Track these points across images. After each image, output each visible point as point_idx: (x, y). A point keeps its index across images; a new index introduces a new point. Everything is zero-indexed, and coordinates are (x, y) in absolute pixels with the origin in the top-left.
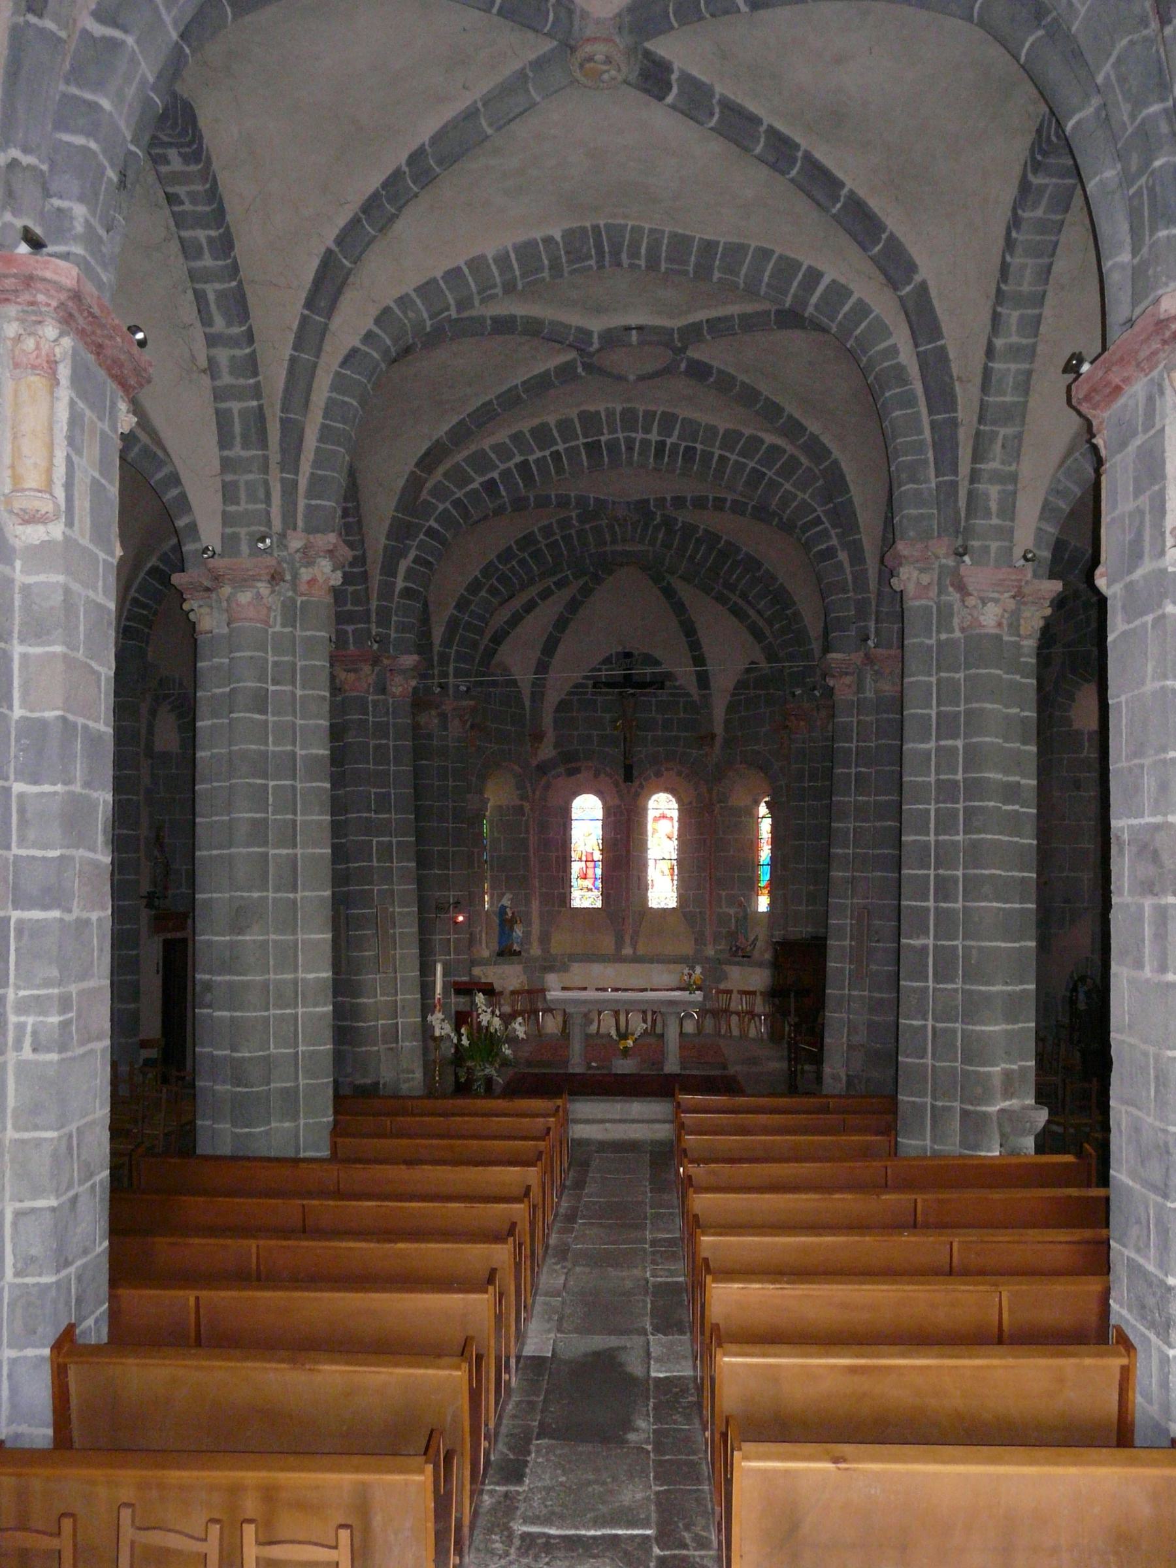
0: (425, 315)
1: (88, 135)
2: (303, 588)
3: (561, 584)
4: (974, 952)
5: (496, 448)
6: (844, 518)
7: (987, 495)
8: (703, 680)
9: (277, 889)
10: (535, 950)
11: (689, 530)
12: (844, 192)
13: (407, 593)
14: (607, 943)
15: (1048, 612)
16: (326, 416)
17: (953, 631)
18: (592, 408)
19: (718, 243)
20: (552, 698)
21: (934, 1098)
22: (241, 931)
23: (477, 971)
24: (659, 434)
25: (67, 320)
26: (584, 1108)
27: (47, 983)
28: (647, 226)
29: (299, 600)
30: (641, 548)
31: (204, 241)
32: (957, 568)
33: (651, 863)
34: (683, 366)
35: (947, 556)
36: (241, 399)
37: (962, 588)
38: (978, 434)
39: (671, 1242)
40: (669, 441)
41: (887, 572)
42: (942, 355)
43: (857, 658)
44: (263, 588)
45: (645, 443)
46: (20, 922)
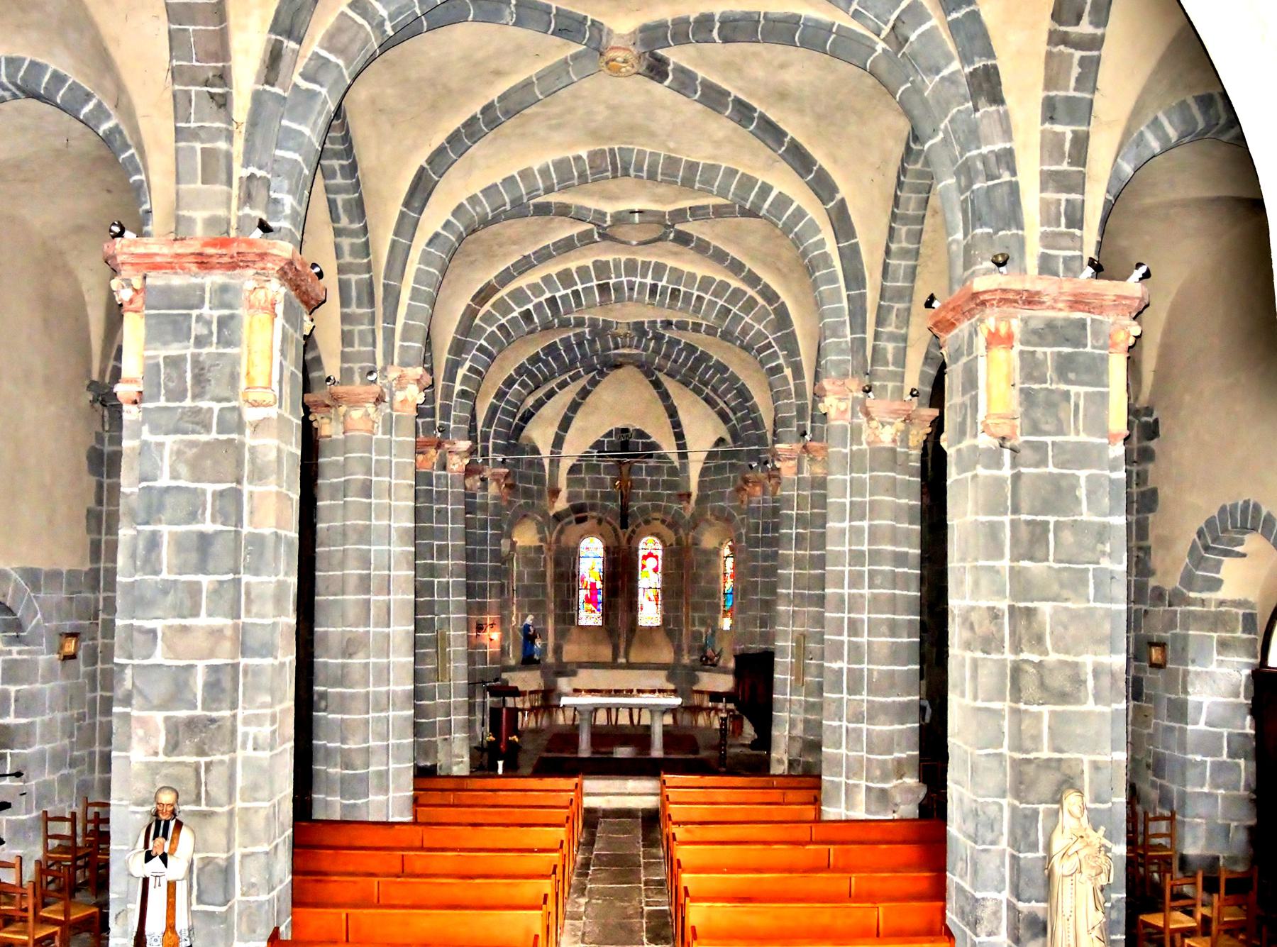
0: (489, 210)
1: (295, 151)
2: (397, 405)
3: (573, 379)
4: (875, 674)
5: (531, 287)
6: (789, 343)
7: (885, 349)
8: (683, 456)
9: (376, 625)
10: (550, 658)
11: (673, 343)
12: (787, 140)
13: (463, 394)
14: (605, 653)
15: (929, 430)
16: (416, 281)
17: (861, 444)
18: (603, 258)
19: (698, 164)
20: (565, 465)
21: (847, 778)
22: (350, 656)
23: (504, 676)
24: (653, 279)
25: (283, 274)
26: (590, 784)
27: (263, 706)
28: (648, 150)
29: (395, 414)
30: (635, 351)
31: (337, 168)
32: (864, 400)
33: (641, 591)
34: (672, 236)
35: (857, 391)
36: (357, 273)
37: (867, 414)
38: (880, 307)
39: (660, 883)
40: (660, 284)
41: (819, 396)
42: (855, 249)
43: (797, 447)
44: (370, 408)
45: (642, 285)
46: (246, 666)
